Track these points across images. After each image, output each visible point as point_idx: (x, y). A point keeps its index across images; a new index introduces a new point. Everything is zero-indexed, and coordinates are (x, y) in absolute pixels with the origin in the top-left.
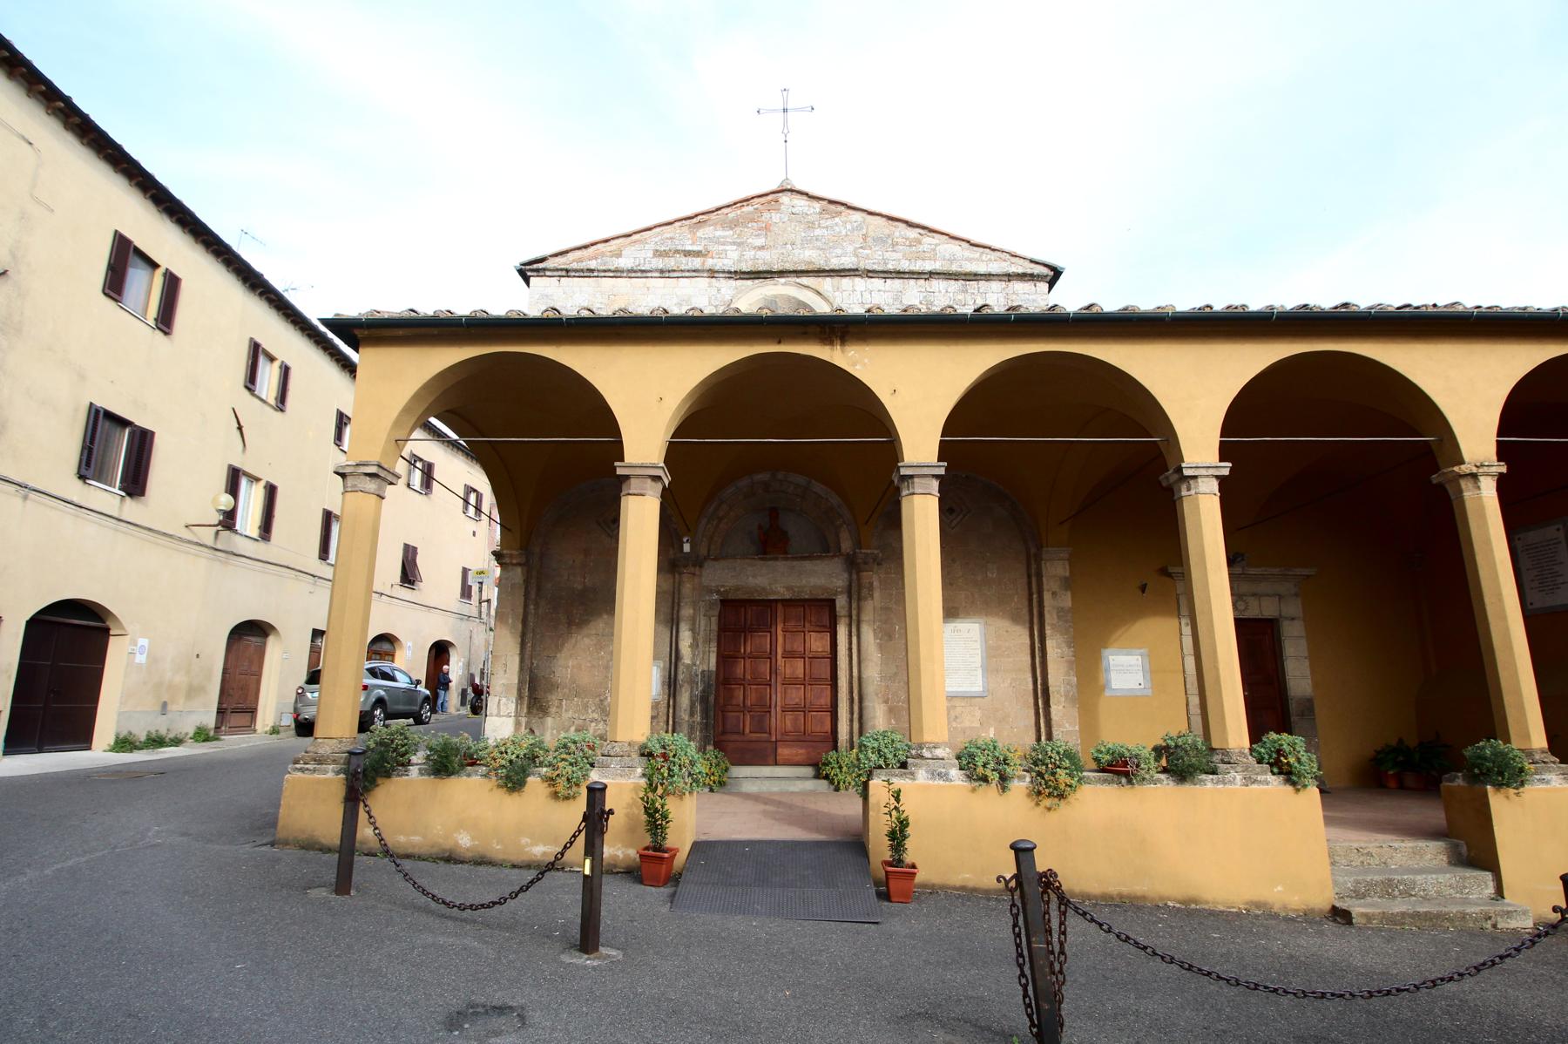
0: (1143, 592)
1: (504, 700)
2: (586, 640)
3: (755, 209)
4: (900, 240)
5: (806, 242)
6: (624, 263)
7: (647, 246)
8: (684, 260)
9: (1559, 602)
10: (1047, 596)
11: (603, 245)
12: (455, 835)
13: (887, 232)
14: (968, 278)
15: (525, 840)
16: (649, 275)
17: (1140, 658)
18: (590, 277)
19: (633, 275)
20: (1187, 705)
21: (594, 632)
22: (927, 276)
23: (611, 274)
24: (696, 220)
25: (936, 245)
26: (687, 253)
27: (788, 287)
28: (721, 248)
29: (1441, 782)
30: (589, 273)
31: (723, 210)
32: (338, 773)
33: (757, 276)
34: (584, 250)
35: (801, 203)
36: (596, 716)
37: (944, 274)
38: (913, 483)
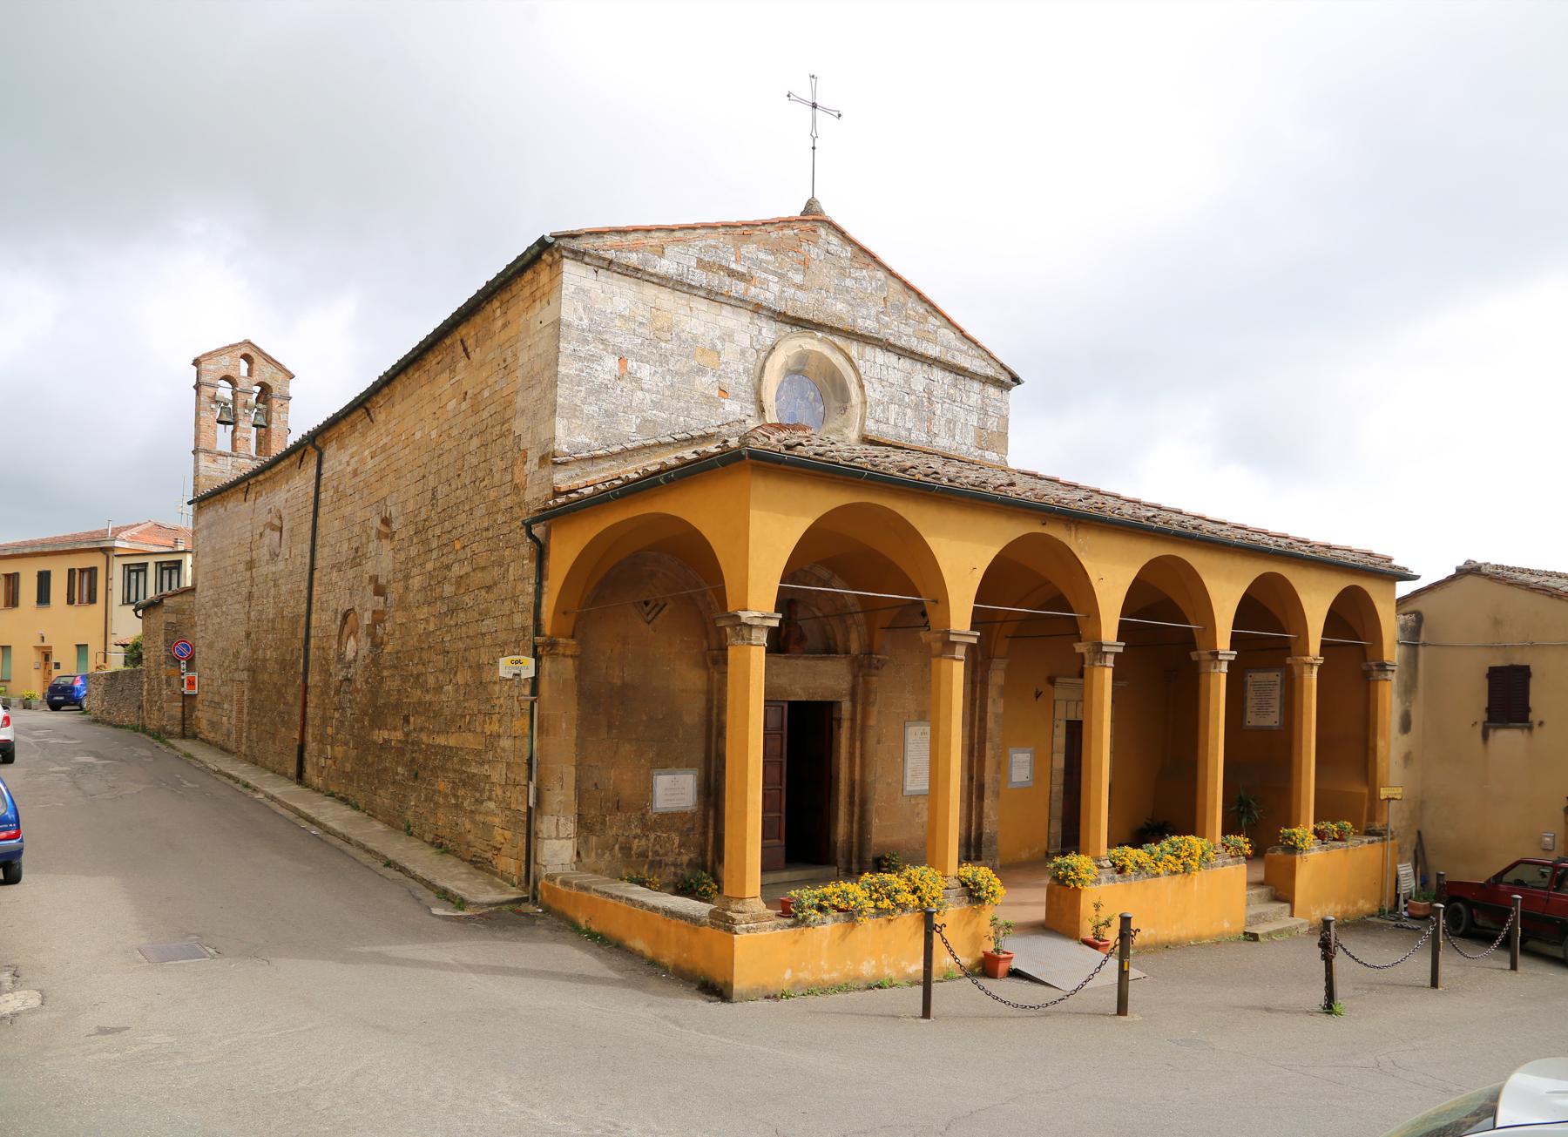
1: (562, 820)
4: (912, 313)
5: (841, 290)
6: (666, 266)
8: (727, 280)
9: (654, 511)
10: (990, 702)
18: (630, 276)
21: (634, 736)
23: (655, 280)
24: (742, 231)
25: (938, 327)
26: (732, 273)
29: (1265, 852)
31: (766, 227)
36: (639, 831)
38: (1105, 657)
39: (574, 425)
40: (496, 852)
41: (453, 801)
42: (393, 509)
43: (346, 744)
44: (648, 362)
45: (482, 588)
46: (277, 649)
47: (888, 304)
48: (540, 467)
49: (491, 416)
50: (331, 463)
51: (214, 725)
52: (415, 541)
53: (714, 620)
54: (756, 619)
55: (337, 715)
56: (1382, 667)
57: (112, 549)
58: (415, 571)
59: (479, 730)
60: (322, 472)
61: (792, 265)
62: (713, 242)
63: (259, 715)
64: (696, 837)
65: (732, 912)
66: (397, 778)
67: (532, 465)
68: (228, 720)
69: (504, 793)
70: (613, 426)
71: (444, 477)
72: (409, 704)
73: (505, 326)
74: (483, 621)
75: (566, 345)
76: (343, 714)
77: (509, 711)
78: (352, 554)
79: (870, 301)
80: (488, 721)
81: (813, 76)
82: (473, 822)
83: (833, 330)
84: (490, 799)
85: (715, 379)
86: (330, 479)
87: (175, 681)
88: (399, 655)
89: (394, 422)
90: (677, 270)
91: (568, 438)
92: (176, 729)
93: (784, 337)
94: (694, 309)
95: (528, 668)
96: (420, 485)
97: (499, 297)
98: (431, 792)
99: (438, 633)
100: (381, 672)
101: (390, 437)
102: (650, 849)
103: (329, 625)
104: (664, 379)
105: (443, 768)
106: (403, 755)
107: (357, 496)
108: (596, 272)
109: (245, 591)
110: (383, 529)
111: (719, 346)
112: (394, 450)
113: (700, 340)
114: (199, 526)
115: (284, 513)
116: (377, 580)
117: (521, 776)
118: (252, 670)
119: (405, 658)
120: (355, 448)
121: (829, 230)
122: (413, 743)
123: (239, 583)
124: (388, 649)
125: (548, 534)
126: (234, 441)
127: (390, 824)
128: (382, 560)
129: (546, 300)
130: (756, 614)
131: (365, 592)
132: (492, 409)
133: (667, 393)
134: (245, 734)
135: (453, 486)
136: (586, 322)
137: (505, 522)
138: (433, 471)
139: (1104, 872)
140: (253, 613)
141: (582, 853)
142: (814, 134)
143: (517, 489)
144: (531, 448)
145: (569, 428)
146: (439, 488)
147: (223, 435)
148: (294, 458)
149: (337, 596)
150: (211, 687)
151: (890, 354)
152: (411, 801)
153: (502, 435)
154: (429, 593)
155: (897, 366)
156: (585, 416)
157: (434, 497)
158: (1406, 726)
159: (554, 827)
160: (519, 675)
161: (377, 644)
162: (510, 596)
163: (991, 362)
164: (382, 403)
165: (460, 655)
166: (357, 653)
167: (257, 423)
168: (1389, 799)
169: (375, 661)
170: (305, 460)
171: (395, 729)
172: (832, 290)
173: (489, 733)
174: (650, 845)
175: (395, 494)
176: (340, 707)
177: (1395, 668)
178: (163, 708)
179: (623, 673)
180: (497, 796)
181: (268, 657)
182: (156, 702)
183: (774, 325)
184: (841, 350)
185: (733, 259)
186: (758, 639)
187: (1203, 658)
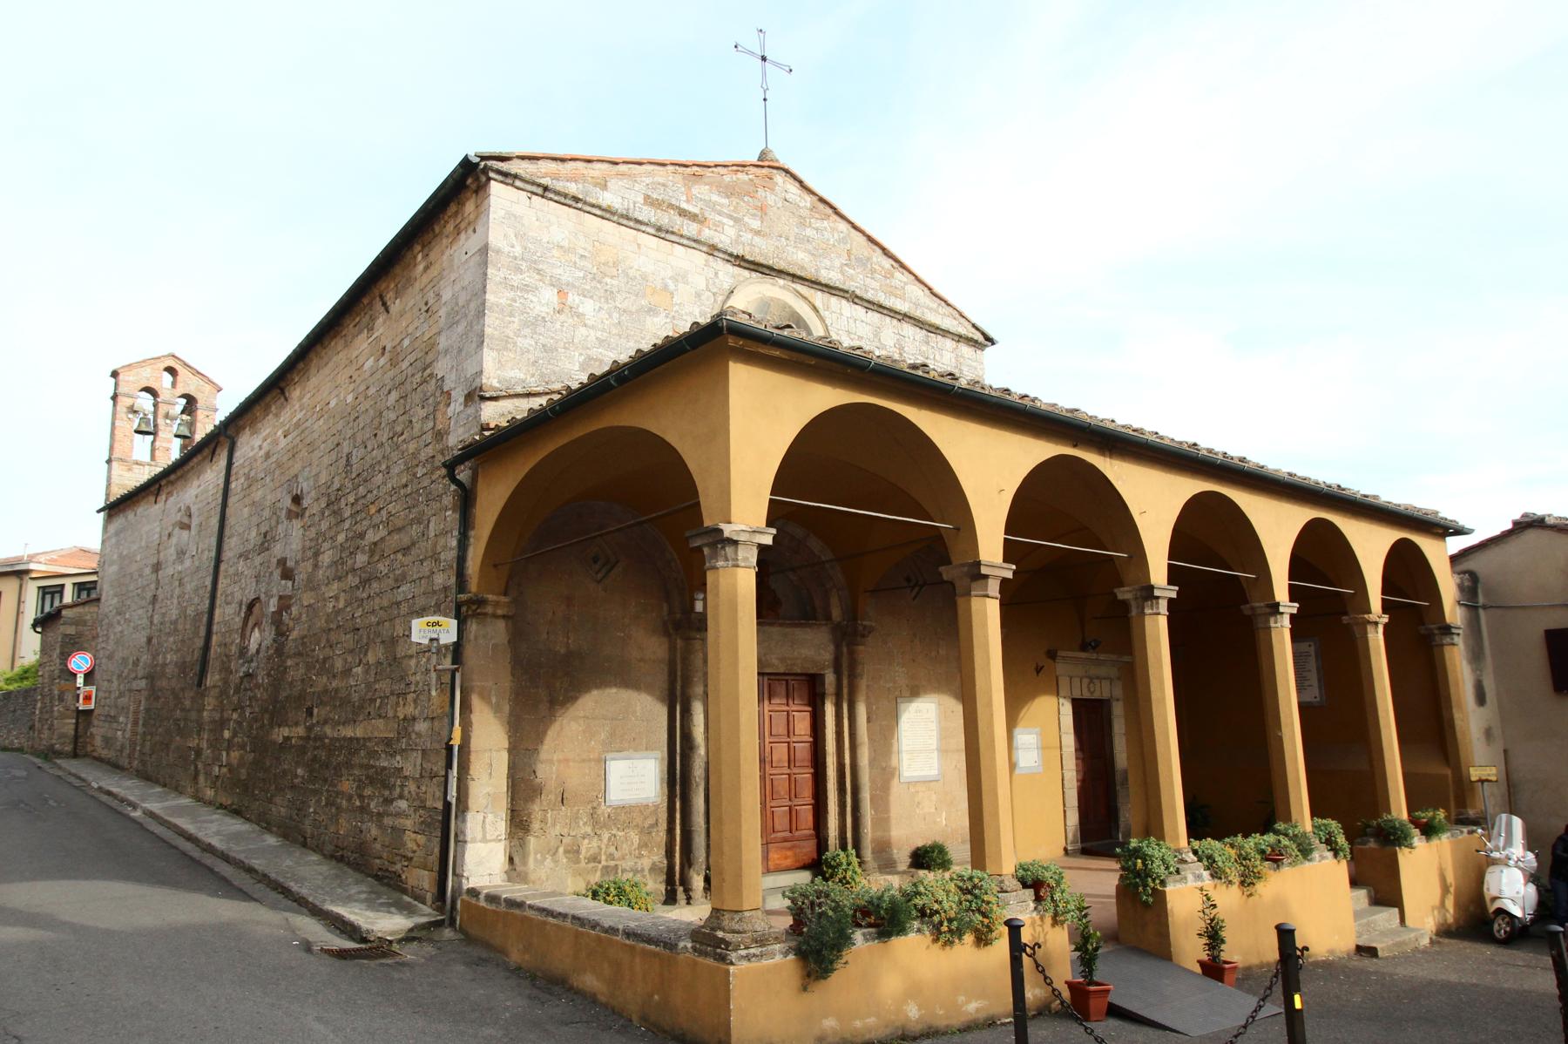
0: (1038, 672)
1: (490, 817)
2: (574, 726)
3: (750, 179)
4: (877, 267)
5: (803, 240)
6: (607, 198)
7: (637, 187)
8: (678, 220)
11: (585, 164)
12: (905, 1008)
13: (866, 254)
14: (930, 329)
15: (961, 999)
16: (643, 228)
17: (1035, 736)
18: (569, 206)
19: (625, 222)
20: (1063, 780)
21: (582, 714)
22: (900, 317)
23: (598, 212)
24: (694, 170)
25: (906, 284)
26: (683, 213)
27: (785, 292)
28: (718, 218)
30: (574, 201)
31: (719, 169)
32: (786, 954)
33: (755, 268)
34: (559, 163)
35: (793, 188)
37: (915, 319)
38: (1158, 603)
39: (505, 358)
40: (406, 864)
41: (358, 803)
42: (305, 485)
43: (242, 747)
44: (591, 297)
45: (398, 551)
46: (178, 650)
47: (852, 257)
48: (466, 406)
49: (411, 364)
50: (243, 450)
51: (107, 741)
52: (326, 514)
53: (687, 539)
54: (742, 534)
55: (235, 716)
56: (1447, 630)
57: (27, 572)
58: (326, 545)
59: (391, 714)
60: (234, 460)
61: (748, 210)
62: (661, 180)
63: (155, 725)
64: (661, 835)
65: (724, 930)
66: (296, 781)
67: (457, 405)
68: (123, 734)
69: (419, 788)
70: (552, 361)
71: (359, 440)
72: (314, 693)
73: (427, 268)
74: (399, 587)
75: (495, 272)
76: (242, 715)
77: (426, 688)
78: (260, 540)
79: (833, 253)
80: (401, 703)
81: (761, 31)
82: (381, 826)
83: (795, 277)
84: (401, 797)
85: (668, 320)
86: (243, 466)
87: (69, 697)
88: (305, 640)
89: (309, 395)
90: (622, 204)
91: (499, 372)
92: (66, 748)
93: (743, 281)
94: (642, 246)
95: (448, 631)
96: (333, 455)
97: (420, 241)
98: (334, 795)
99: (348, 609)
100: (284, 662)
101: (304, 412)
102: (603, 851)
103: (232, 619)
104: (610, 316)
105: (349, 765)
106: (305, 753)
107: (268, 479)
108: (529, 198)
109: (149, 595)
110: (294, 508)
111: (672, 287)
112: (308, 424)
113: (651, 279)
114: (108, 534)
115: (194, 509)
116: (286, 562)
117: (439, 767)
118: (151, 677)
119: (310, 643)
120: (267, 431)
121: (787, 179)
122: (316, 739)
123: (143, 588)
124: (294, 635)
125: (474, 478)
126: (153, 450)
127: (285, 836)
128: (292, 540)
129: (472, 229)
130: (743, 527)
131: (272, 578)
132: (411, 358)
133: (614, 331)
134: (138, 748)
135: (369, 448)
136: (518, 250)
137: (426, 474)
138: (348, 437)
139: (1190, 868)
140: (156, 617)
141: (516, 860)
142: (764, 86)
143: (440, 435)
144: (455, 388)
145: (500, 361)
146: (354, 453)
147: (142, 445)
148: (206, 452)
149: (243, 586)
150: (108, 700)
151: (857, 306)
152: (310, 807)
153: (424, 381)
154: (340, 567)
155: (864, 319)
156: (519, 349)
157: (348, 463)
158: (1481, 699)
159: (479, 828)
160: (437, 640)
161: (281, 632)
162: (431, 554)
163: (963, 320)
164: (296, 380)
165: (373, 630)
166: (260, 645)
167: (179, 433)
168: (1482, 781)
169: (279, 650)
170: (217, 453)
171: (297, 724)
172: (792, 238)
173: (402, 717)
174: (603, 846)
175: (308, 469)
176: (238, 707)
177: (1460, 631)
178: (53, 725)
179: (568, 638)
180: (410, 792)
181: (168, 661)
182: (47, 720)
183: (729, 267)
184: (805, 298)
185: (684, 198)
186: (746, 559)
187: (1259, 611)
